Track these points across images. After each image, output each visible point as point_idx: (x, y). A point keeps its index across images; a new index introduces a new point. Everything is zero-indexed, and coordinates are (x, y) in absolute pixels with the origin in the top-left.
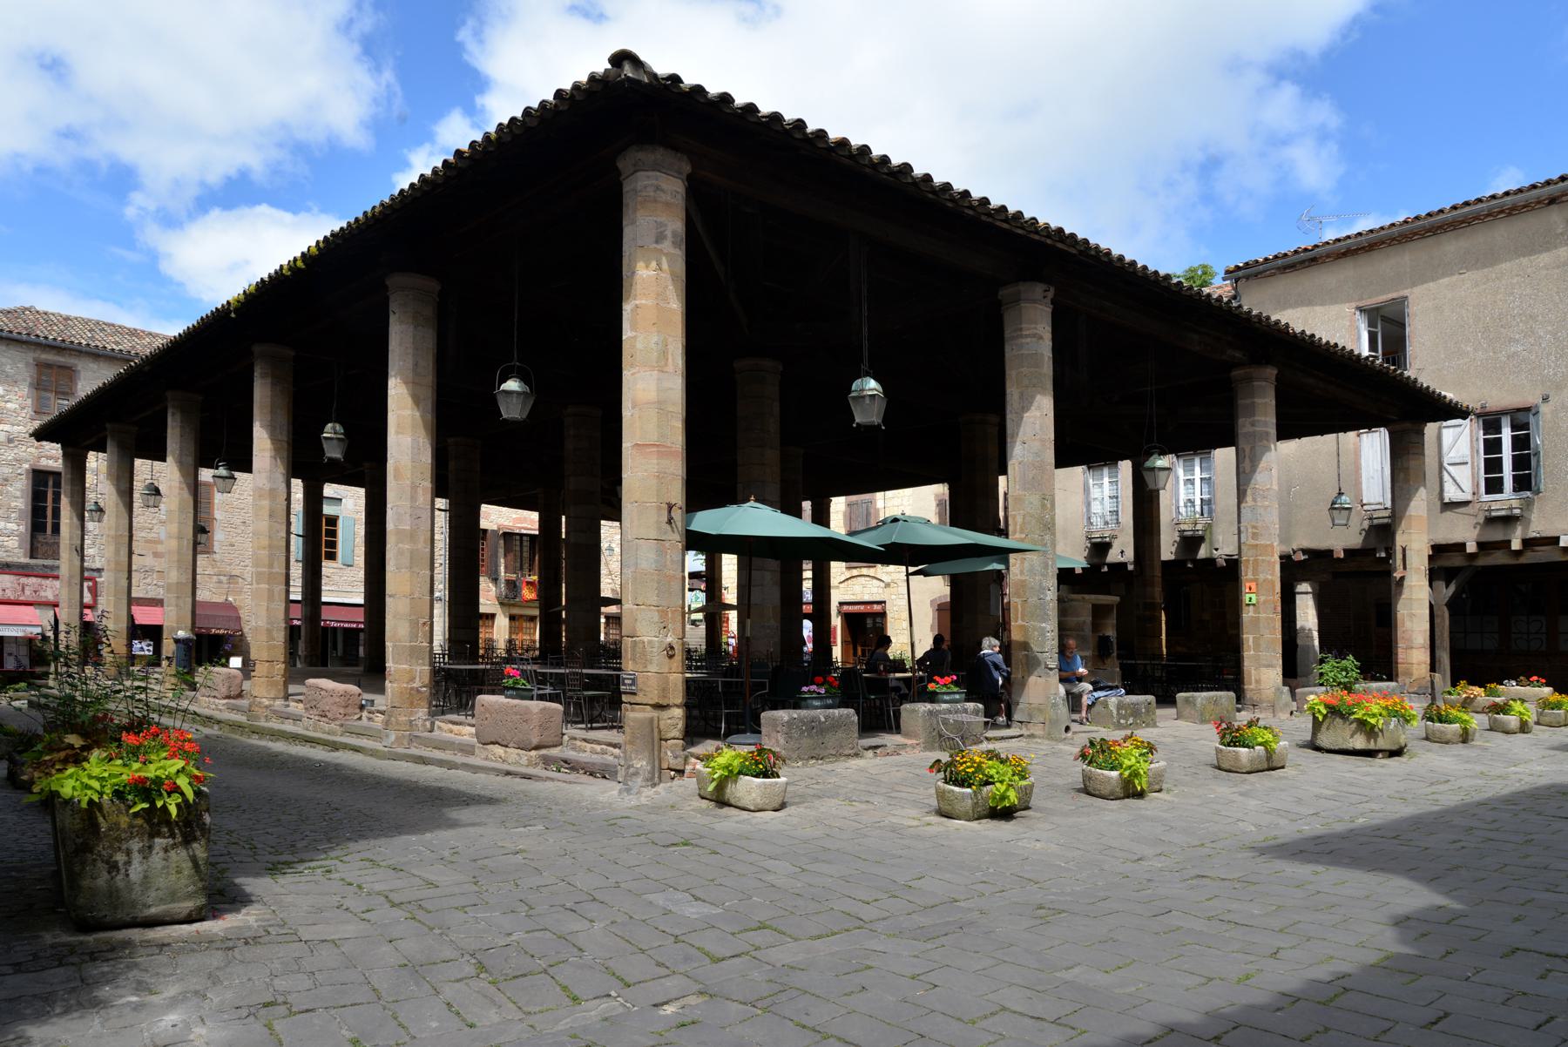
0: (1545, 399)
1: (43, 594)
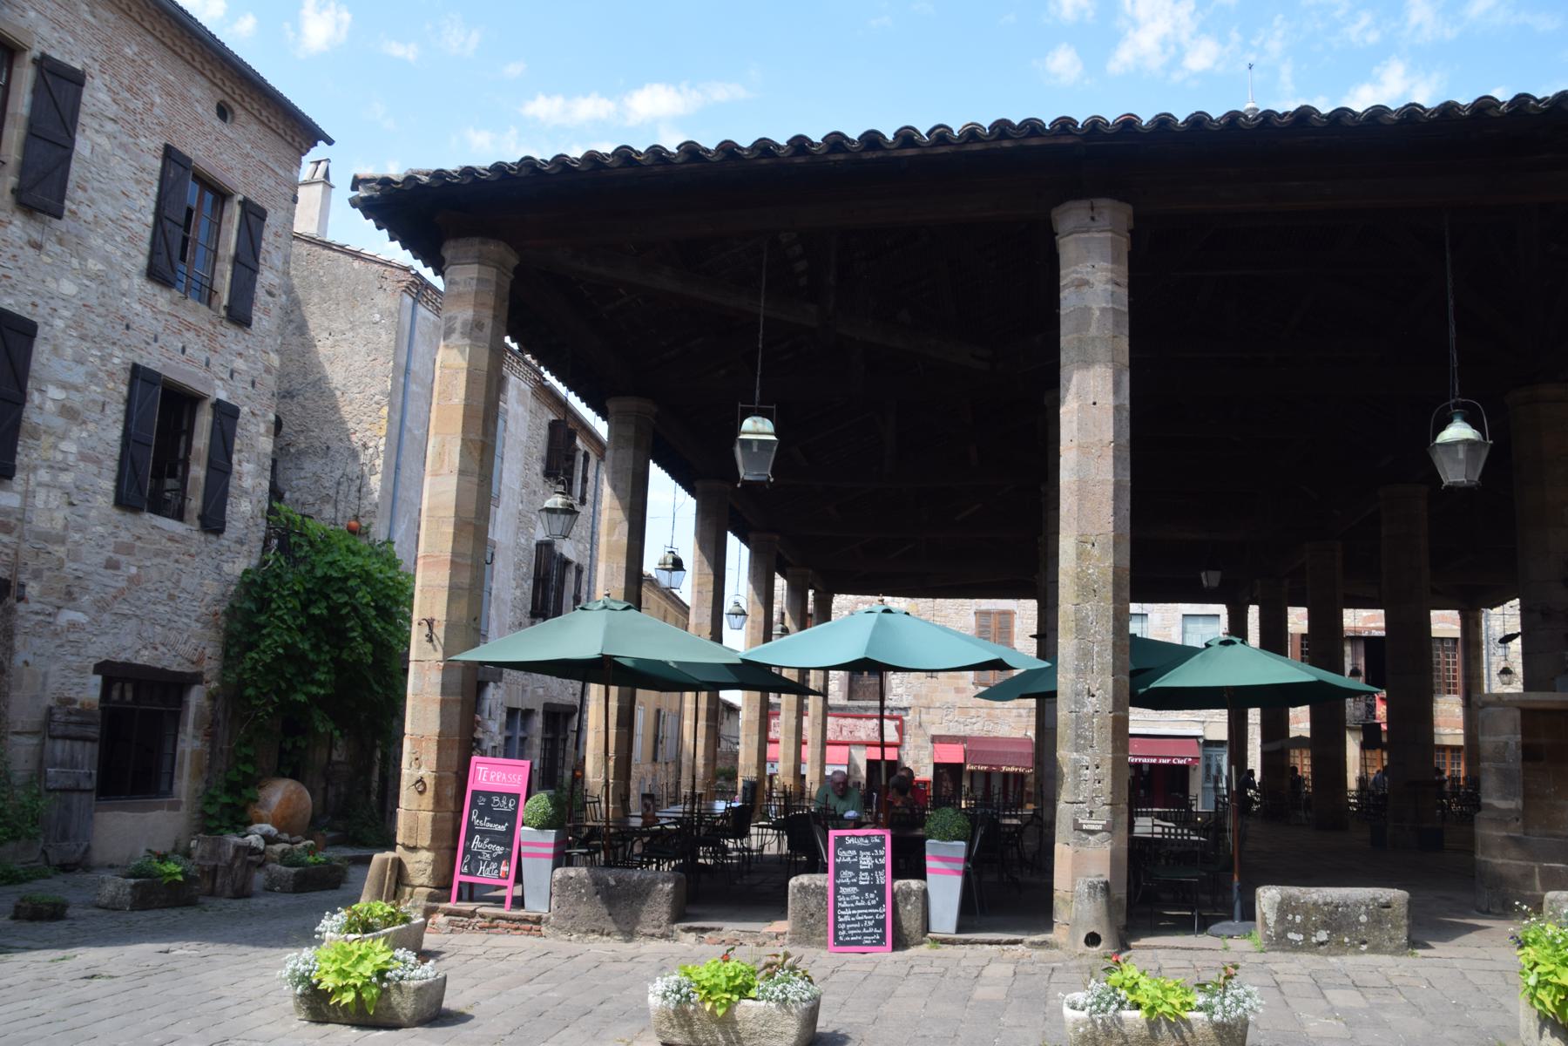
1: (857, 734)
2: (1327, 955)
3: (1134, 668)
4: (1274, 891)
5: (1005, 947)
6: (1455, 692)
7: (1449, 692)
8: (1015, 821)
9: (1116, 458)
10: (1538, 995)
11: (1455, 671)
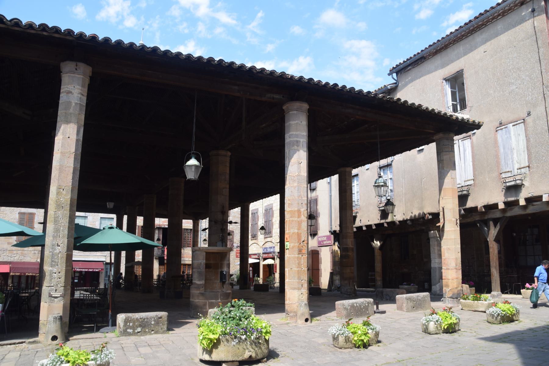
0: (529, 114)
2: (140, 336)
3: (76, 236)
4: (123, 315)
5: (17, 345)
6: (190, 247)
7: (188, 247)
8: (27, 295)
9: (75, 159)
10: (203, 342)
11: (190, 240)
